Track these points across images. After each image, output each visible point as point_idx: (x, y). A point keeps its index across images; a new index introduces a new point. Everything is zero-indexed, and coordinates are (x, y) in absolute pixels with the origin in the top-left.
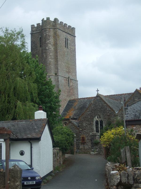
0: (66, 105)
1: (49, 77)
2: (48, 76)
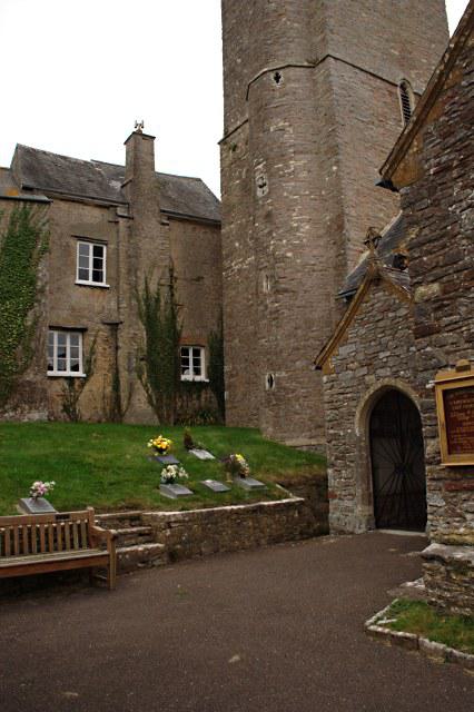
0: (394, 220)
1: (277, 78)
2: (272, 75)
